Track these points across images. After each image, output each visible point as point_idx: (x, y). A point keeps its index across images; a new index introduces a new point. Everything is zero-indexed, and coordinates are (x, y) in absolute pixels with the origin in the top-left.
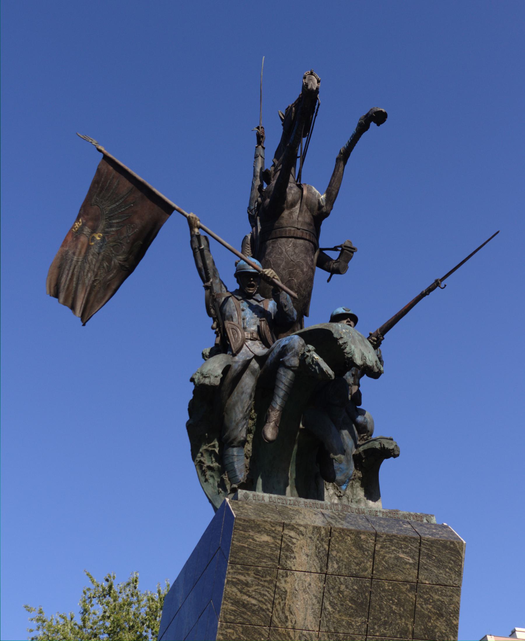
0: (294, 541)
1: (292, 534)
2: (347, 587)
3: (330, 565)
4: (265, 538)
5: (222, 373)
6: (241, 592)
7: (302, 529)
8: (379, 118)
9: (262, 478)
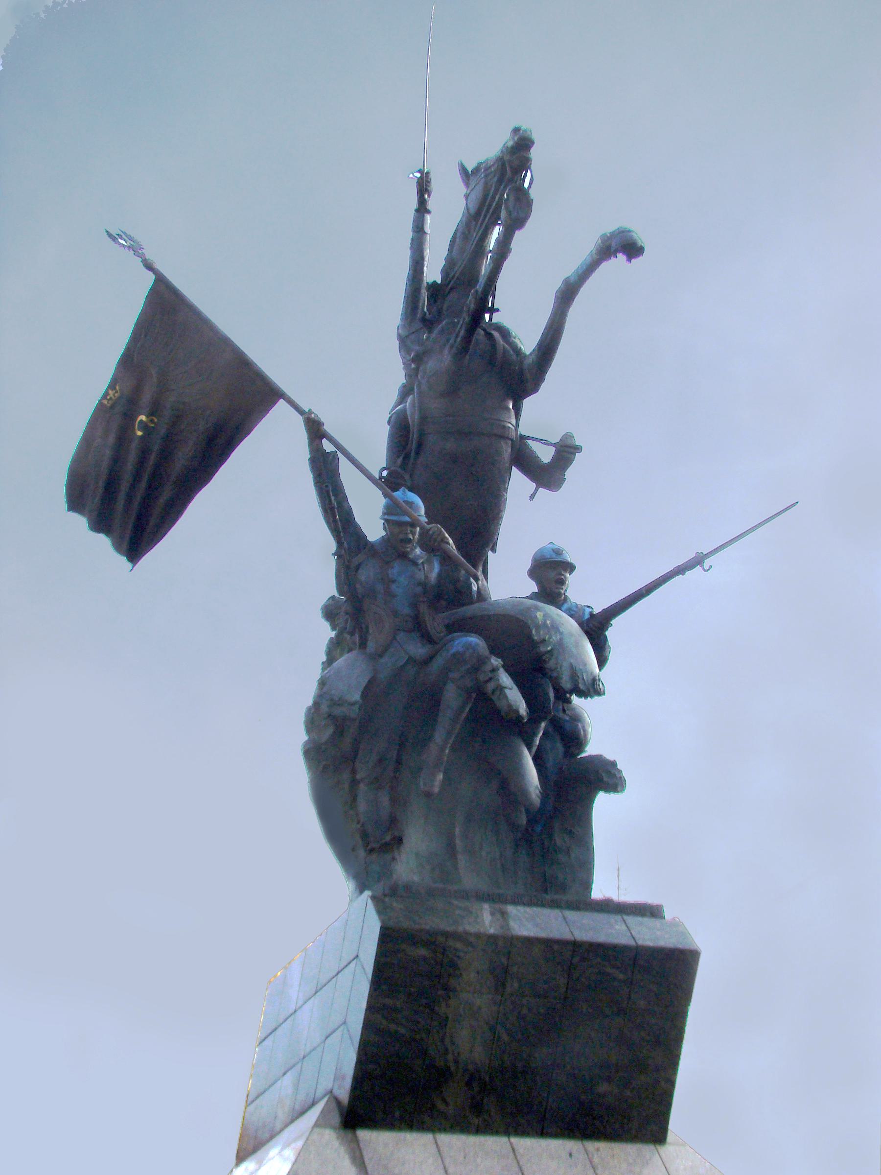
0: (462, 954)
1: (459, 945)
2: (530, 1010)
3: (508, 985)
4: (423, 952)
5: (362, 696)
6: (387, 1019)
7: (472, 939)
8: (631, 249)
9: (521, 717)
